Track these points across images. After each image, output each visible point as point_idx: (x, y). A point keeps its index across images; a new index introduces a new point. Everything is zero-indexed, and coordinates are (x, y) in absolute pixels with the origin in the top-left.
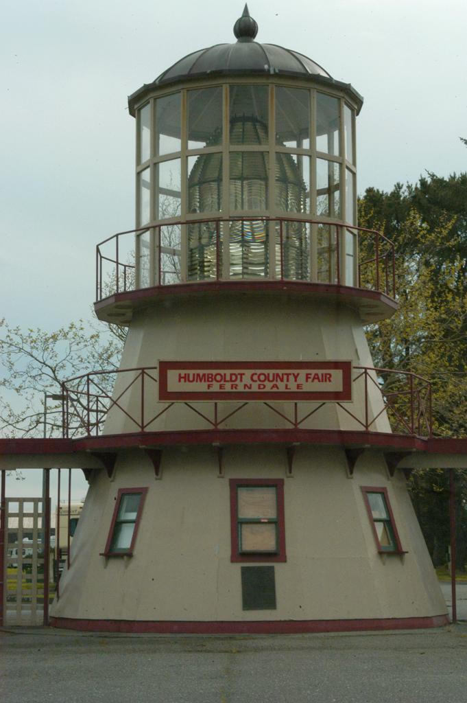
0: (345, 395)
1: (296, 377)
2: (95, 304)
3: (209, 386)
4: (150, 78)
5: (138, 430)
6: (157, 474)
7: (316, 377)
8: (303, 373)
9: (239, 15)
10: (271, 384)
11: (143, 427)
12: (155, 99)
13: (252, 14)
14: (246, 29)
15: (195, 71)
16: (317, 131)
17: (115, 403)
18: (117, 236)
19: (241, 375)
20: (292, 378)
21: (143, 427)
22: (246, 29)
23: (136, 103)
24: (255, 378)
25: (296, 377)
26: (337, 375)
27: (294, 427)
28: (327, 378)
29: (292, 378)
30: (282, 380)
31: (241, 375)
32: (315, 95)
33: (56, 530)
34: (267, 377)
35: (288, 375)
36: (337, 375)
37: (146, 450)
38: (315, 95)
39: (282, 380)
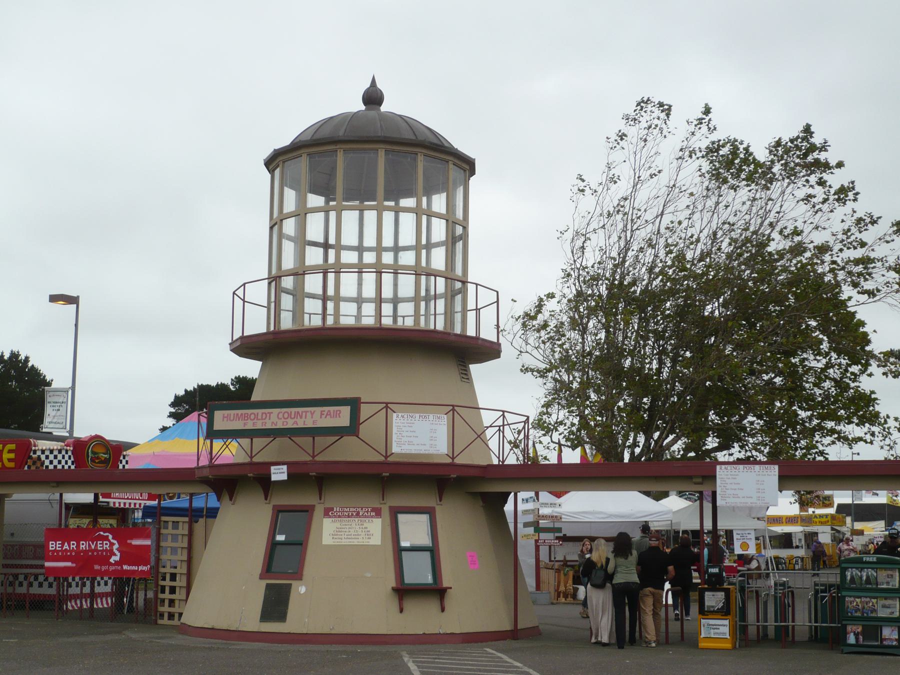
0: (353, 429)
1: (312, 414)
2: (230, 344)
3: (245, 424)
4: (285, 141)
5: (248, 460)
6: (266, 499)
7: (329, 414)
8: (318, 410)
9: (368, 85)
10: (293, 421)
11: (251, 457)
12: (284, 162)
13: (379, 85)
14: (373, 98)
15: (316, 137)
16: (424, 188)
17: (479, 436)
18: (244, 285)
19: (270, 413)
20: (309, 415)
21: (453, 458)
22: (373, 98)
23: (273, 162)
24: (281, 416)
25: (312, 414)
26: (346, 411)
27: (383, 459)
28: (338, 414)
29: (309, 415)
30: (301, 417)
31: (270, 413)
32: (420, 158)
33: (153, 553)
34: (290, 415)
35: (306, 412)
36: (346, 411)
37: (254, 478)
38: (420, 158)
39: (301, 417)
